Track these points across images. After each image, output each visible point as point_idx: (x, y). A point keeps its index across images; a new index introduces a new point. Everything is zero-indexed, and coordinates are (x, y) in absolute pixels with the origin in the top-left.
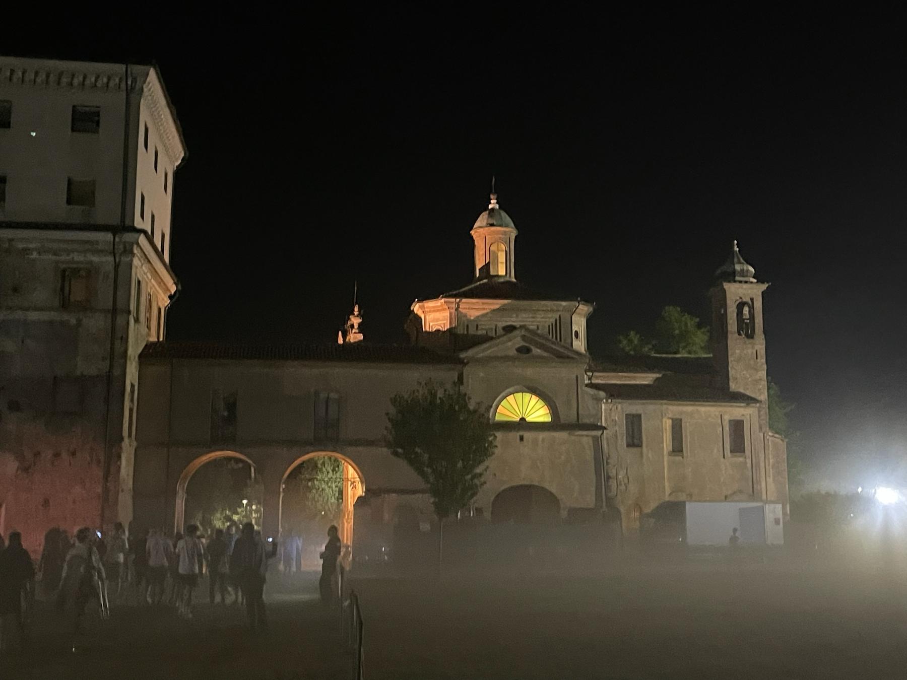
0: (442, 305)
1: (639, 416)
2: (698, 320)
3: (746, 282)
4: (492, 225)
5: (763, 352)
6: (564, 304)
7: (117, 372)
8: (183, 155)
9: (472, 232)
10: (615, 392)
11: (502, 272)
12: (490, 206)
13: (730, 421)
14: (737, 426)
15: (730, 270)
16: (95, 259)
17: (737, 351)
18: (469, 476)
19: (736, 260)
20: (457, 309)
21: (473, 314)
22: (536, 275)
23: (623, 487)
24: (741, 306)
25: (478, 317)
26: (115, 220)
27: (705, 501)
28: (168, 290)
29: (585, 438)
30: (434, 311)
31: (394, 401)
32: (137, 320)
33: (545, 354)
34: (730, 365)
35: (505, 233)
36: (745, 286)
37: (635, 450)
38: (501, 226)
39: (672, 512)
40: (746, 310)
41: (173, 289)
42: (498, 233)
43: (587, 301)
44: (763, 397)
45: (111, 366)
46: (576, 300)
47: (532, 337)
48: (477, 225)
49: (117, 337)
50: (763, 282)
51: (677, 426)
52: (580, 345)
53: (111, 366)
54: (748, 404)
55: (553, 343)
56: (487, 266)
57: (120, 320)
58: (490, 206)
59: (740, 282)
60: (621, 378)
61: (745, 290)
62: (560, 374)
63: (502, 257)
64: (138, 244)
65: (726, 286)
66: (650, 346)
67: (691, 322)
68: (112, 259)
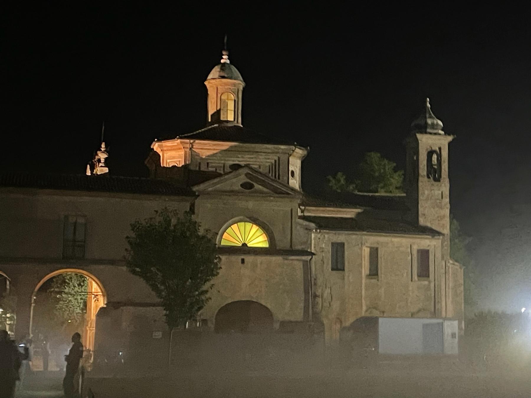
1: (342, 245)
2: (395, 164)
3: (435, 134)
4: (223, 77)
6: (283, 147)
9: (206, 83)
10: (324, 224)
11: (231, 118)
12: (222, 61)
14: (424, 254)
15: (422, 122)
18: (197, 293)
19: (428, 115)
22: (259, 124)
24: (430, 154)
25: (208, 156)
29: (296, 263)
31: (133, 227)
33: (265, 190)
34: (420, 202)
35: (234, 85)
36: (434, 137)
39: (367, 325)
40: (435, 157)
42: (226, 84)
43: (301, 145)
44: (446, 231)
48: (210, 77)
50: (449, 135)
51: (374, 253)
52: (295, 183)
55: (272, 180)
56: (218, 112)
58: (222, 61)
61: (434, 141)
62: (278, 207)
65: (419, 136)
66: (354, 186)
67: (389, 166)
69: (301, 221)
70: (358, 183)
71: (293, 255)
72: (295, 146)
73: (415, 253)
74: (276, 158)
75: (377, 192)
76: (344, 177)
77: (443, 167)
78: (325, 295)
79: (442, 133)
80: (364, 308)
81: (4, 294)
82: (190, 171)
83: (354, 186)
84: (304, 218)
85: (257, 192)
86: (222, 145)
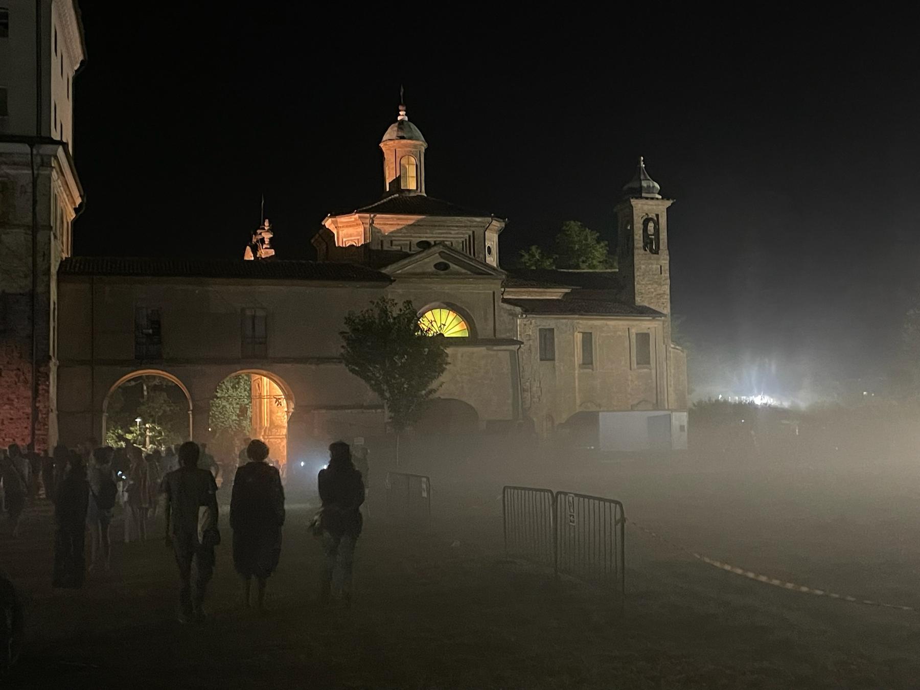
0: (356, 220)
1: (552, 330)
2: (598, 234)
3: (652, 199)
4: (402, 138)
5: (667, 267)
6: (478, 219)
7: (40, 289)
8: (81, 58)
9: (381, 145)
10: (531, 308)
11: (412, 185)
12: (399, 118)
13: (637, 334)
14: (644, 338)
15: (635, 185)
16: (12, 172)
17: (643, 267)
18: (424, 392)
19: (642, 177)
20: (371, 225)
21: (387, 230)
22: (446, 192)
23: (536, 400)
24: (646, 221)
25: (392, 232)
26: (33, 132)
27: (614, 411)
28: (75, 204)
29: (502, 353)
30: (347, 227)
31: (349, 321)
32: (55, 237)
33: (464, 271)
34: (636, 279)
35: (415, 146)
36: (650, 202)
37: (548, 363)
38: (410, 139)
39: (586, 420)
40: (651, 225)
41: (79, 201)
42: (406, 146)
43: (499, 216)
44: (667, 311)
45: (34, 283)
46: (490, 216)
47: (449, 251)
48: (385, 138)
49: (38, 251)
50: (668, 199)
51: (588, 338)
52: (492, 260)
53: (34, 283)
54: (654, 318)
55: (470, 259)
56: (397, 181)
57: (41, 237)
58: (399, 118)
59: (647, 198)
60: (530, 293)
61: (651, 206)
62: (479, 291)
63: (412, 171)
64: (56, 157)
65: (634, 202)
66: (551, 261)
67: (591, 236)
68: (30, 172)
69: (505, 306)
70: (562, 258)
71: (498, 345)
72: (492, 218)
73: (633, 337)
74: (471, 233)
75: (577, 267)
76: (539, 251)
77: (661, 237)
78: (534, 389)
79: (660, 197)
80: (578, 402)
81: (141, 401)
82: (370, 250)
83: (551, 261)
84: (505, 301)
85: (452, 274)
86: (407, 219)
